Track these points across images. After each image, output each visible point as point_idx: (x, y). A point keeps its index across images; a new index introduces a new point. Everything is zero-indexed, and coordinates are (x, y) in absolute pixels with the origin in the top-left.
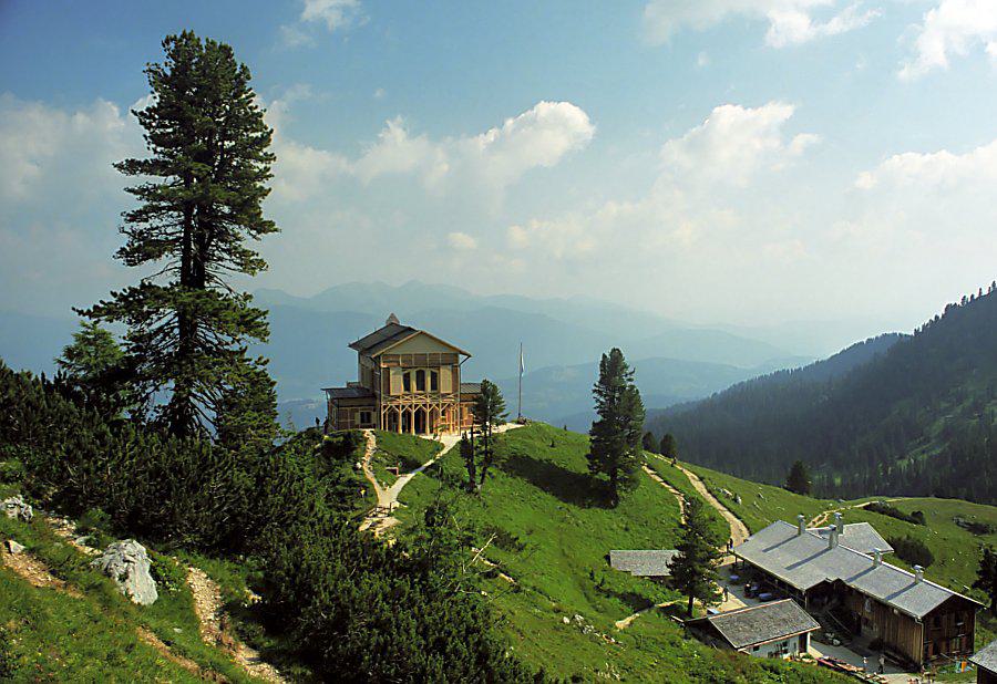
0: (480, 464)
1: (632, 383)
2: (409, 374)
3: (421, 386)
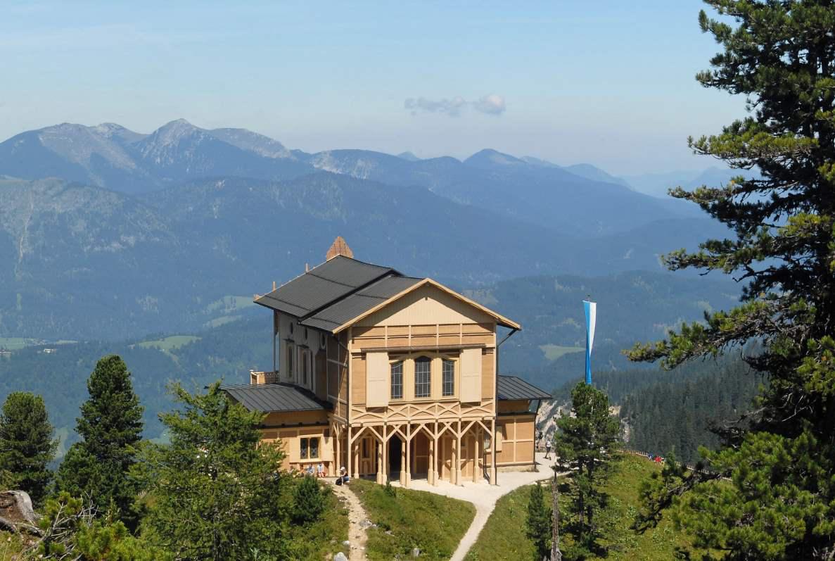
3: (423, 388)
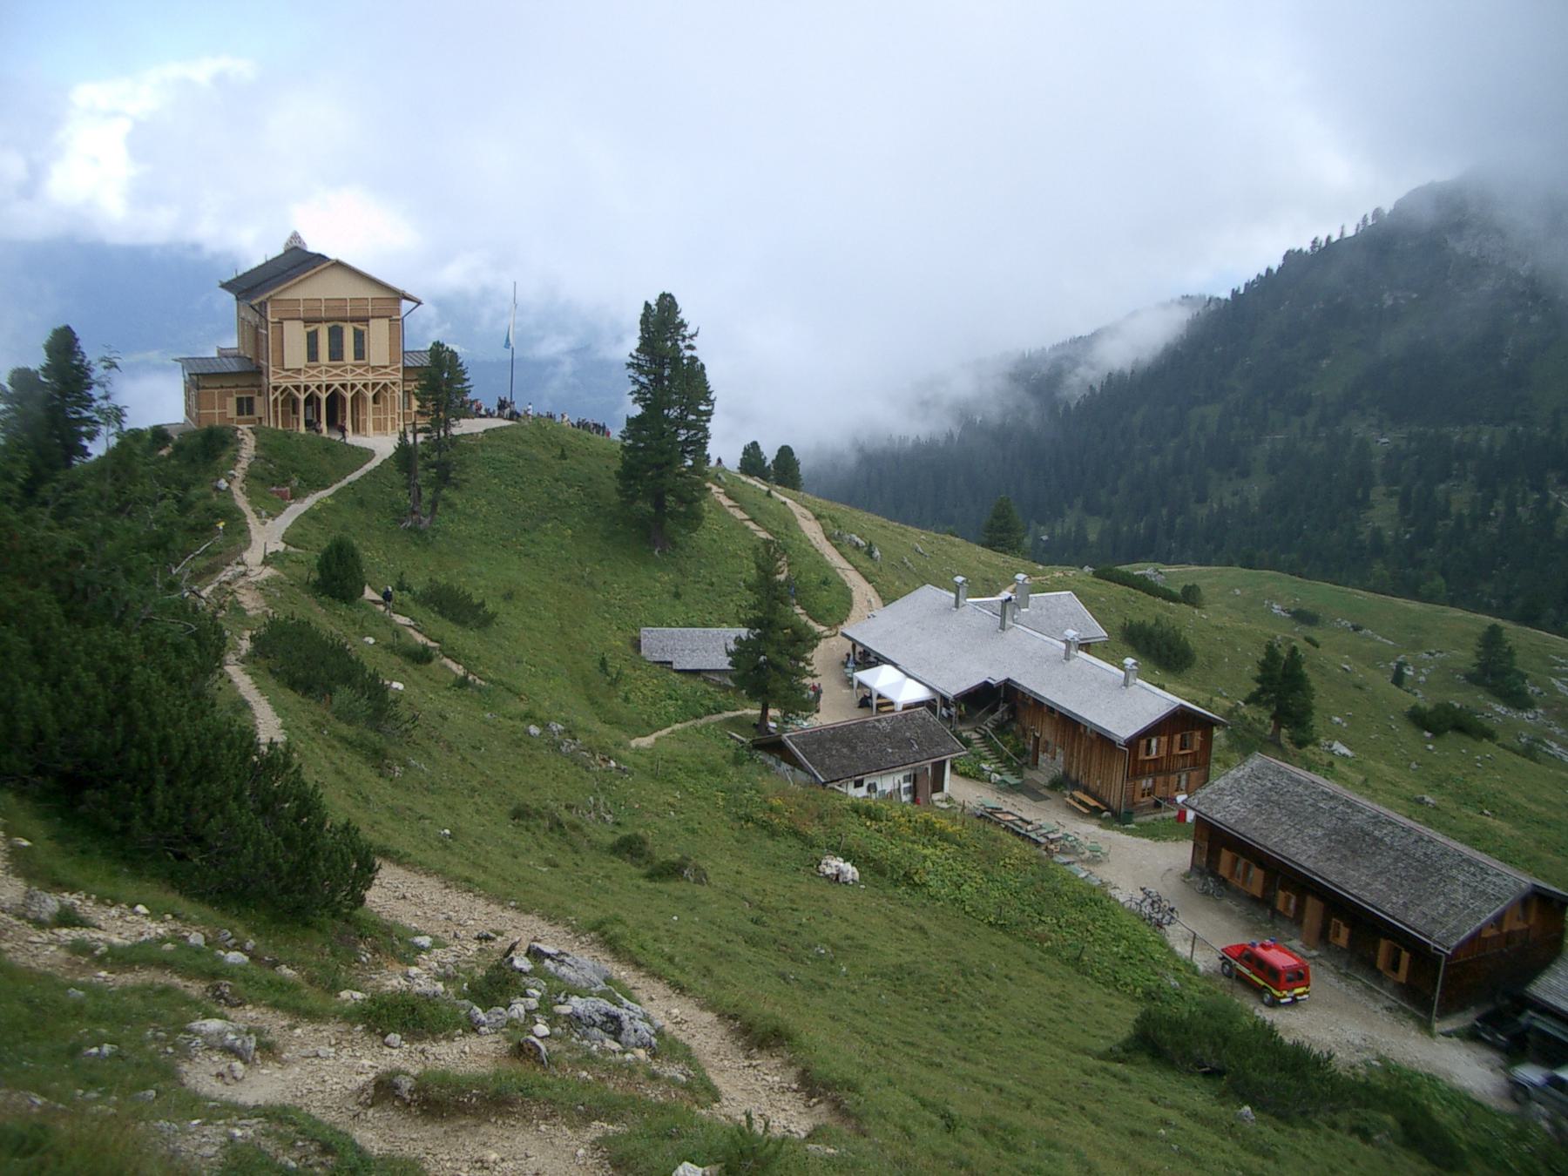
0: (430, 483)
1: (694, 353)
2: (1181, 749)
3: (336, 353)
